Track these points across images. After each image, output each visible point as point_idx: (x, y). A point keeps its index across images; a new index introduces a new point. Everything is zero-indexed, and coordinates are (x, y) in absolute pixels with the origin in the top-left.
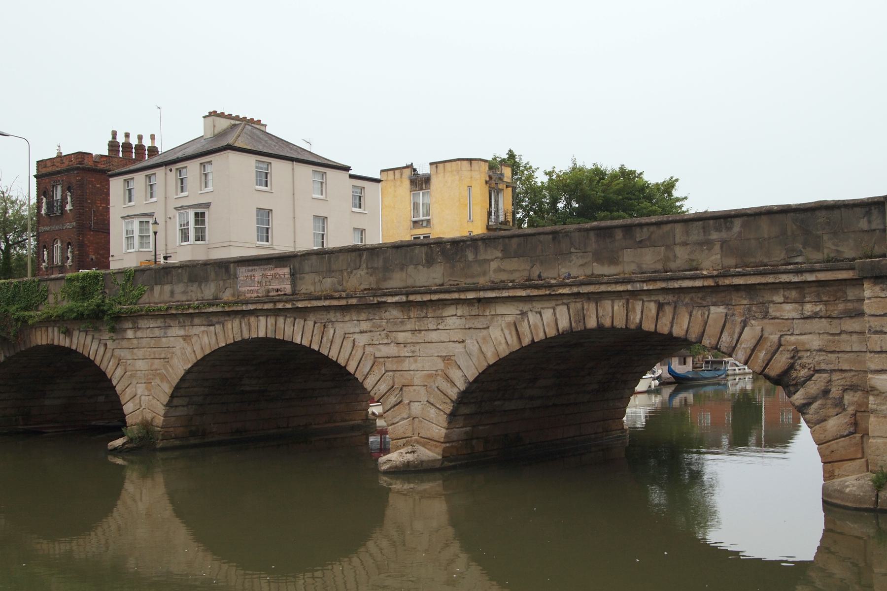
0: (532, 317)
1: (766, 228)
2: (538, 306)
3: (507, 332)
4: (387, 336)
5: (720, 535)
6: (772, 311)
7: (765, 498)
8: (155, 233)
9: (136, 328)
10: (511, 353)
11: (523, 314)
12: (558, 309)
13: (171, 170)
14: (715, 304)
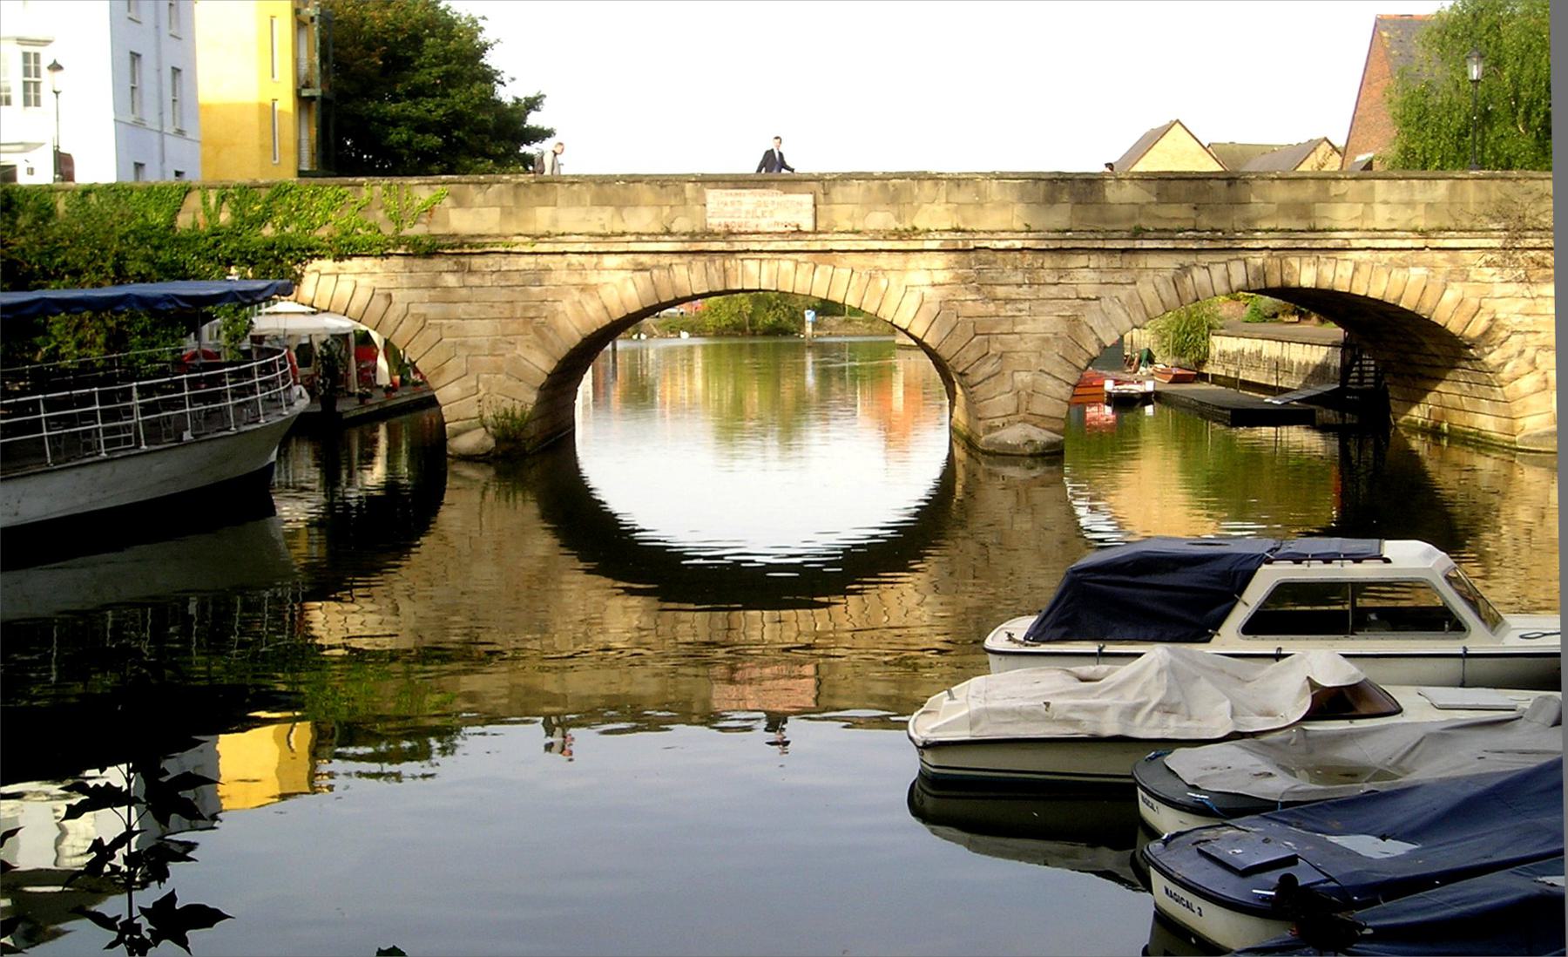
0: (1199, 275)
2: (1204, 259)
4: (978, 290)
6: (1473, 275)
7: (46, 828)
10: (1365, 297)
11: (1185, 269)
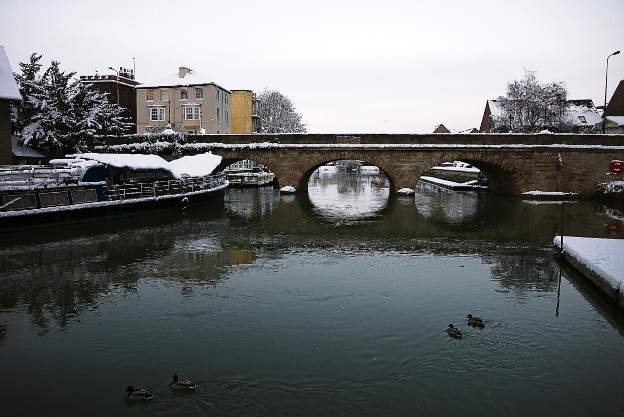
1: (255, 137)
3: (438, 159)
5: (221, 157)
6: (510, 157)
8: (169, 107)
9: (620, 301)
11: (443, 155)
12: (454, 154)
13: (177, 90)
14: (496, 155)
